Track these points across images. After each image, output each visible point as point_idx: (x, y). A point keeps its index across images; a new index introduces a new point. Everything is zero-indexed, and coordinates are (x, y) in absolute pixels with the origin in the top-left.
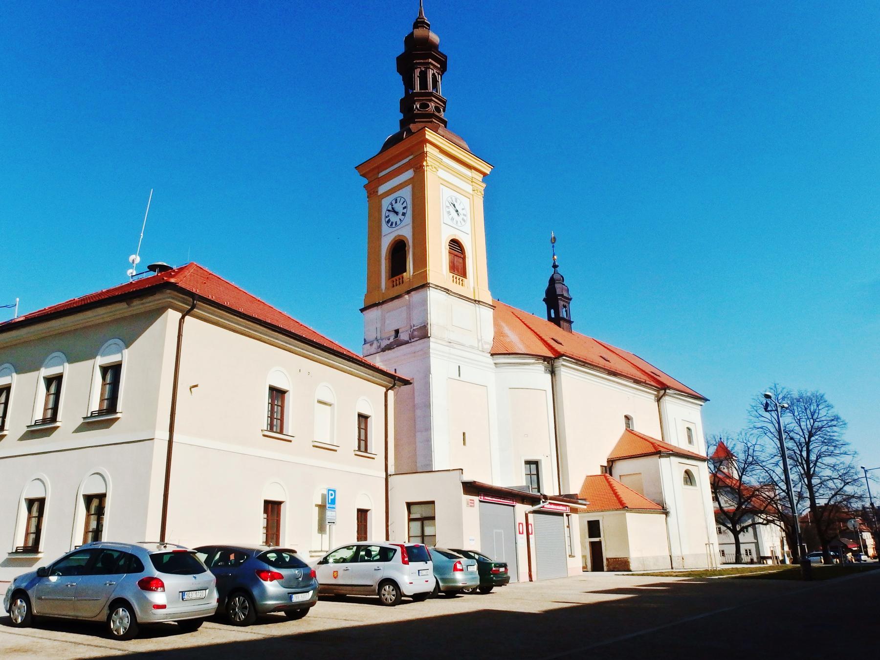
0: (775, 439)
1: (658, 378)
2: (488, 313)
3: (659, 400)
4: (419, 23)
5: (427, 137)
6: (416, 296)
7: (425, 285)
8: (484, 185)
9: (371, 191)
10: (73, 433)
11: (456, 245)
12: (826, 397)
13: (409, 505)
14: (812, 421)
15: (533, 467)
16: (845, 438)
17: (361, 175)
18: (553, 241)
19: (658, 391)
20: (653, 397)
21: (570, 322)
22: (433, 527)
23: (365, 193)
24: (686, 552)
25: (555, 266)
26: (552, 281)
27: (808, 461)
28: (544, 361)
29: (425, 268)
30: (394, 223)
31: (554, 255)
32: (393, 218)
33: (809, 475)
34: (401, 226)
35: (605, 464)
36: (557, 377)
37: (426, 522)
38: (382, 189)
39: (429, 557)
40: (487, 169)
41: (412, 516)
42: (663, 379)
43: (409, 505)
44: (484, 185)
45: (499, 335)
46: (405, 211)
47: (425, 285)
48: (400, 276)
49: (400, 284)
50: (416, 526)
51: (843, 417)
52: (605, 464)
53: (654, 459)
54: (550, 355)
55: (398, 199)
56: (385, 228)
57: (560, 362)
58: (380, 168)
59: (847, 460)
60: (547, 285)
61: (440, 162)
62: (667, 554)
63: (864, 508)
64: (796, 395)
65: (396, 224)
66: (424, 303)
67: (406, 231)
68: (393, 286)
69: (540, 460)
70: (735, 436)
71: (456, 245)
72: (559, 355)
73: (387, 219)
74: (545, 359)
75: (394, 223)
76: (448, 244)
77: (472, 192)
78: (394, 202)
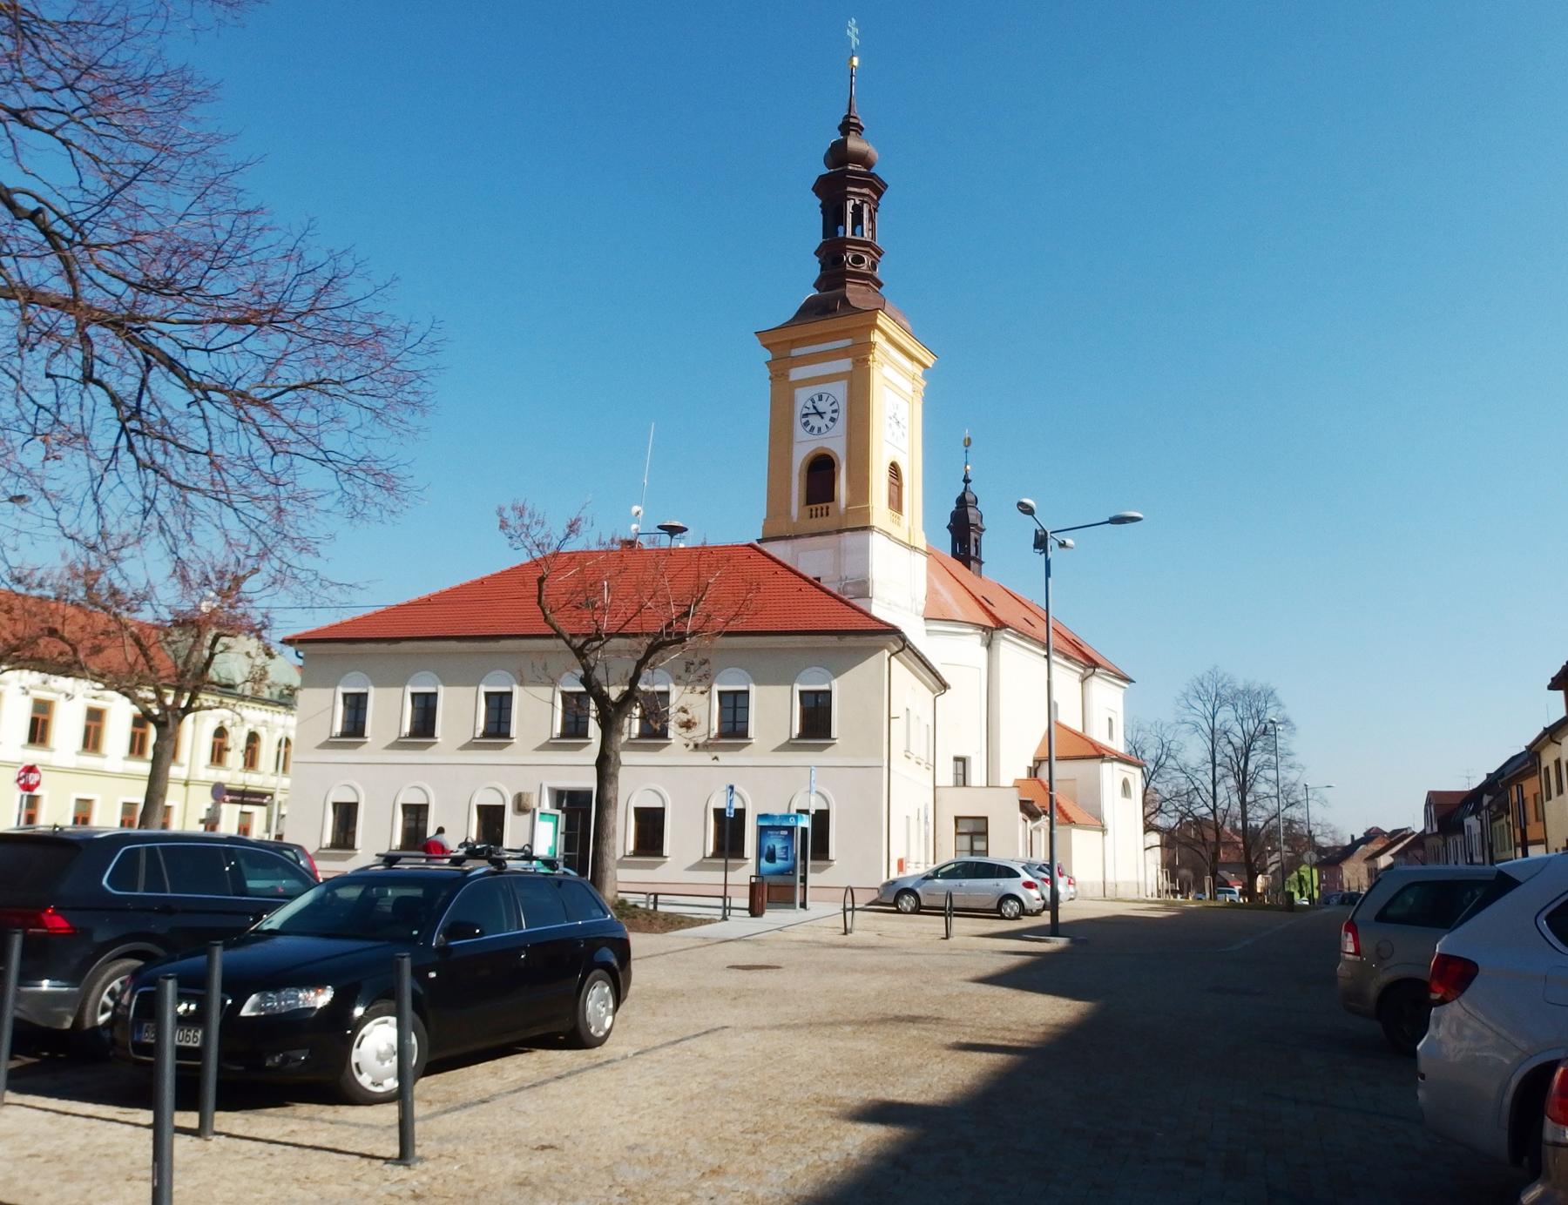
0: (1206, 739)
1: (990, 607)
2: (921, 561)
3: (1084, 680)
4: (848, 126)
5: (879, 322)
6: (849, 539)
7: (867, 528)
8: (924, 383)
9: (779, 370)
10: (774, 751)
11: (895, 469)
12: (1277, 693)
13: (957, 819)
14: (1256, 721)
15: (960, 764)
16: (1293, 747)
17: (764, 346)
18: (968, 442)
19: (1084, 669)
20: (1077, 677)
21: (980, 562)
22: (982, 840)
23: (767, 373)
24: (1119, 879)
25: (967, 481)
26: (962, 502)
27: (1245, 772)
28: (983, 631)
29: (863, 503)
30: (816, 429)
31: (966, 464)
32: (815, 421)
33: (1243, 788)
34: (825, 436)
35: (1031, 765)
36: (994, 651)
37: (975, 837)
38: (797, 374)
39: (312, 879)
40: (929, 361)
41: (959, 830)
42: (1095, 658)
43: (957, 819)
44: (924, 383)
45: (932, 593)
46: (835, 415)
47: (867, 528)
48: (824, 505)
49: (822, 515)
50: (966, 839)
51: (1293, 719)
52: (1031, 765)
53: (1096, 762)
54: (990, 623)
55: (825, 397)
56: (800, 432)
57: (1003, 633)
58: (794, 343)
59: (1293, 776)
60: (953, 506)
61: (886, 353)
62: (1101, 880)
63: (1257, 826)
64: (1240, 686)
65: (820, 429)
66: (864, 550)
67: (835, 444)
68: (811, 517)
69: (970, 758)
70: (1147, 727)
71: (895, 469)
72: (1001, 625)
73: (804, 420)
74: (985, 628)
75: (816, 429)
76: (888, 469)
77: (911, 393)
78: (816, 399)
